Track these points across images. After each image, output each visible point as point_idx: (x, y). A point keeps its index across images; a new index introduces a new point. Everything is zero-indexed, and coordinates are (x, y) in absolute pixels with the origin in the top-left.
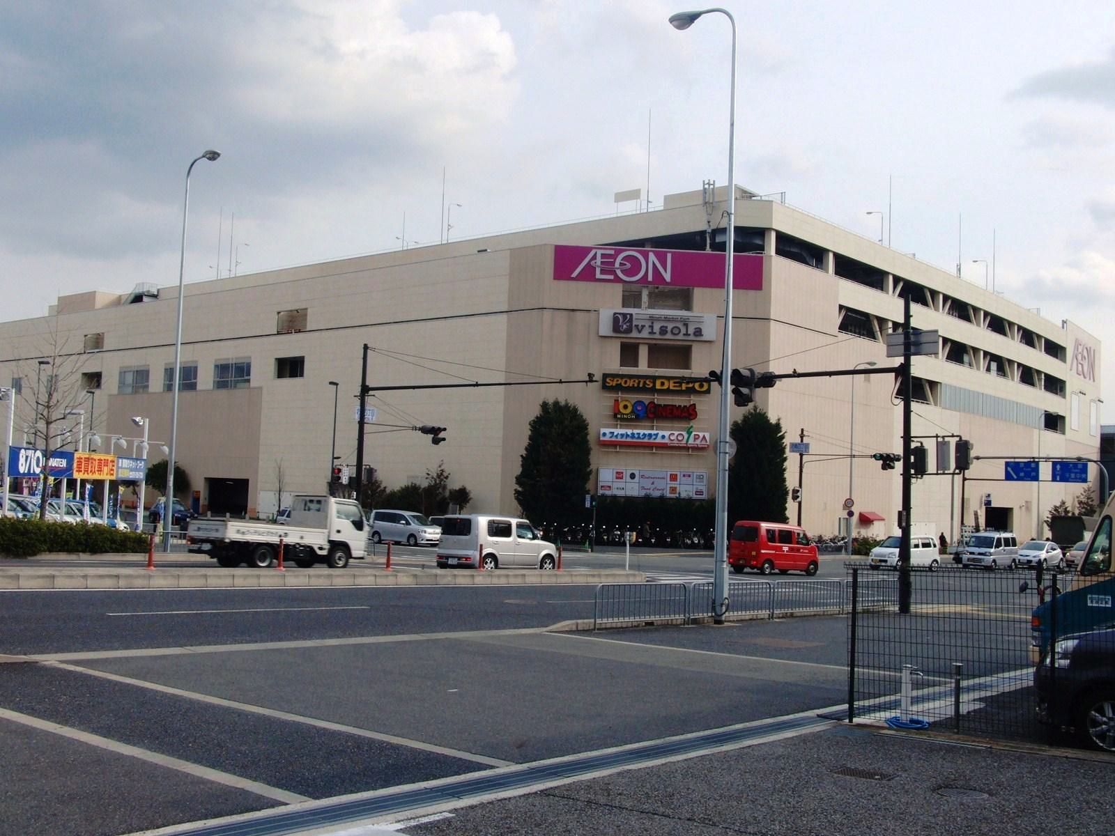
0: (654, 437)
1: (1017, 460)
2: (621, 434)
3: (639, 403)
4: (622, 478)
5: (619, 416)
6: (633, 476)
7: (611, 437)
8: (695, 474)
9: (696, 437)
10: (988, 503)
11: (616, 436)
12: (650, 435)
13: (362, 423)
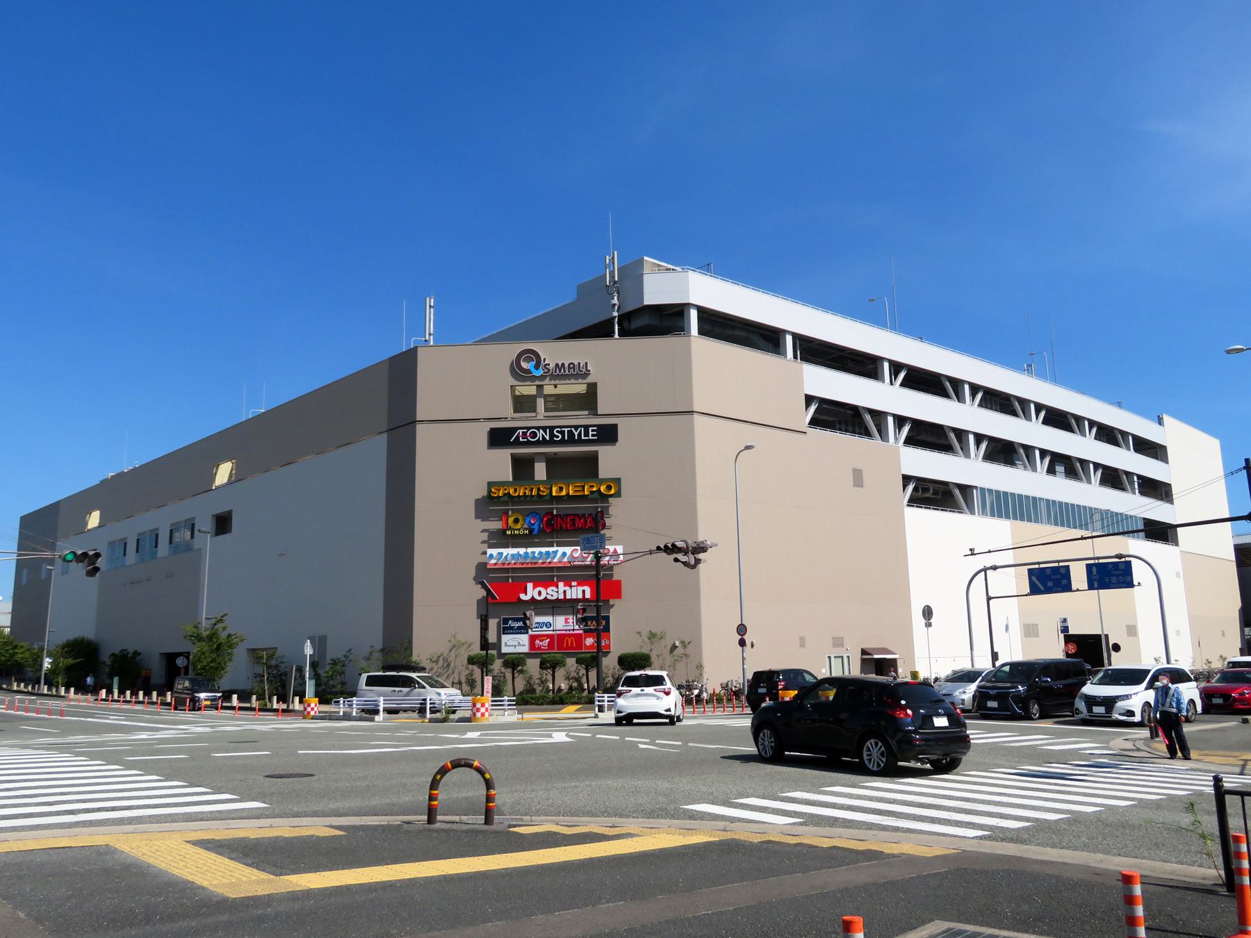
0: (552, 556)
1: (1042, 566)
10: (1065, 629)
13: (1017, 596)
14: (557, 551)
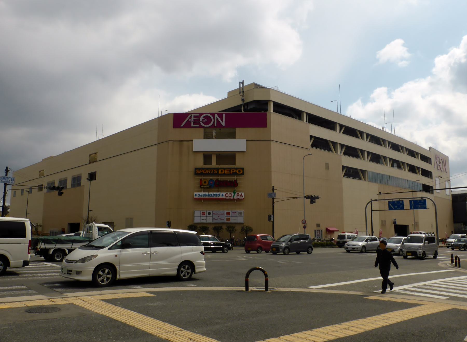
0: (218, 195)
1: (393, 200)
2: (203, 195)
3: (211, 180)
4: (205, 215)
5: (202, 187)
6: (209, 214)
7: (199, 196)
8: (238, 212)
9: (238, 195)
10: (395, 223)
11: (201, 196)
12: (216, 195)
14: (220, 194)
